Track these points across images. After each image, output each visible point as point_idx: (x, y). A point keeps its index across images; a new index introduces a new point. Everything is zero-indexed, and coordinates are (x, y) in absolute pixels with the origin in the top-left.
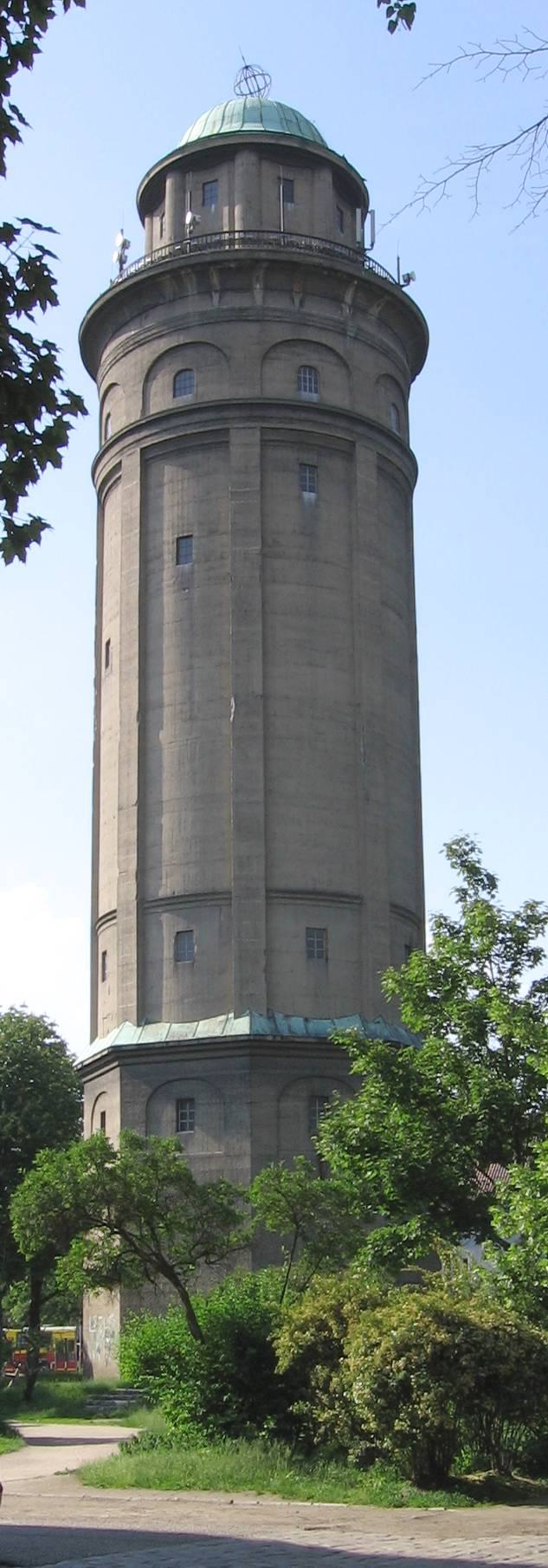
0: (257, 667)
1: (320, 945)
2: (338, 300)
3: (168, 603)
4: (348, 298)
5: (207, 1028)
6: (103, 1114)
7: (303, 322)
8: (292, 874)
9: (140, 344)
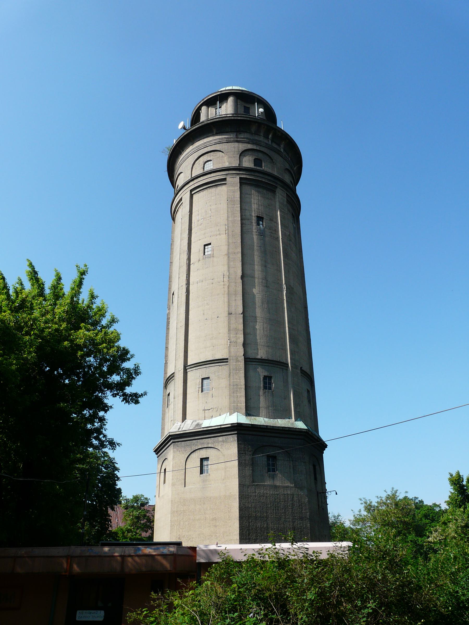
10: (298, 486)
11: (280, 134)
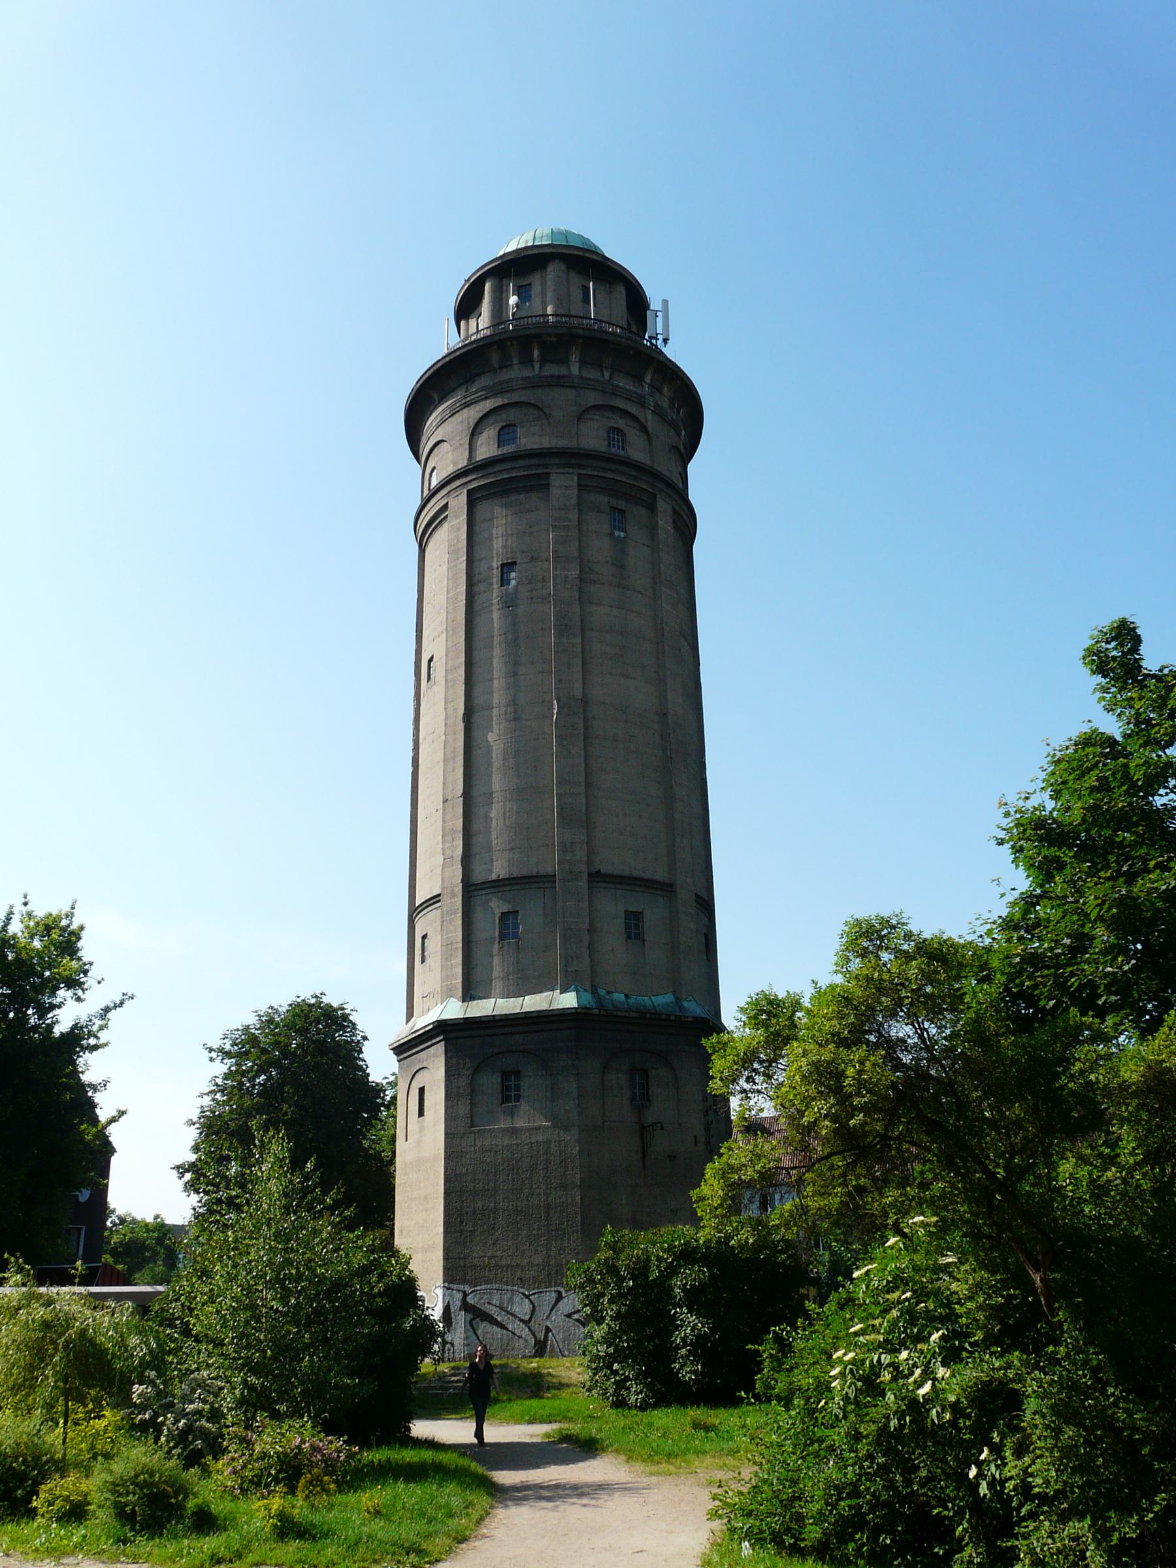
0: (578, 675)
1: (637, 927)
2: (639, 379)
3: (495, 619)
4: (648, 379)
5: (533, 1003)
6: (422, 1090)
7: (615, 392)
8: (612, 862)
9: (467, 405)
10: (559, 1124)
11: (554, 339)
